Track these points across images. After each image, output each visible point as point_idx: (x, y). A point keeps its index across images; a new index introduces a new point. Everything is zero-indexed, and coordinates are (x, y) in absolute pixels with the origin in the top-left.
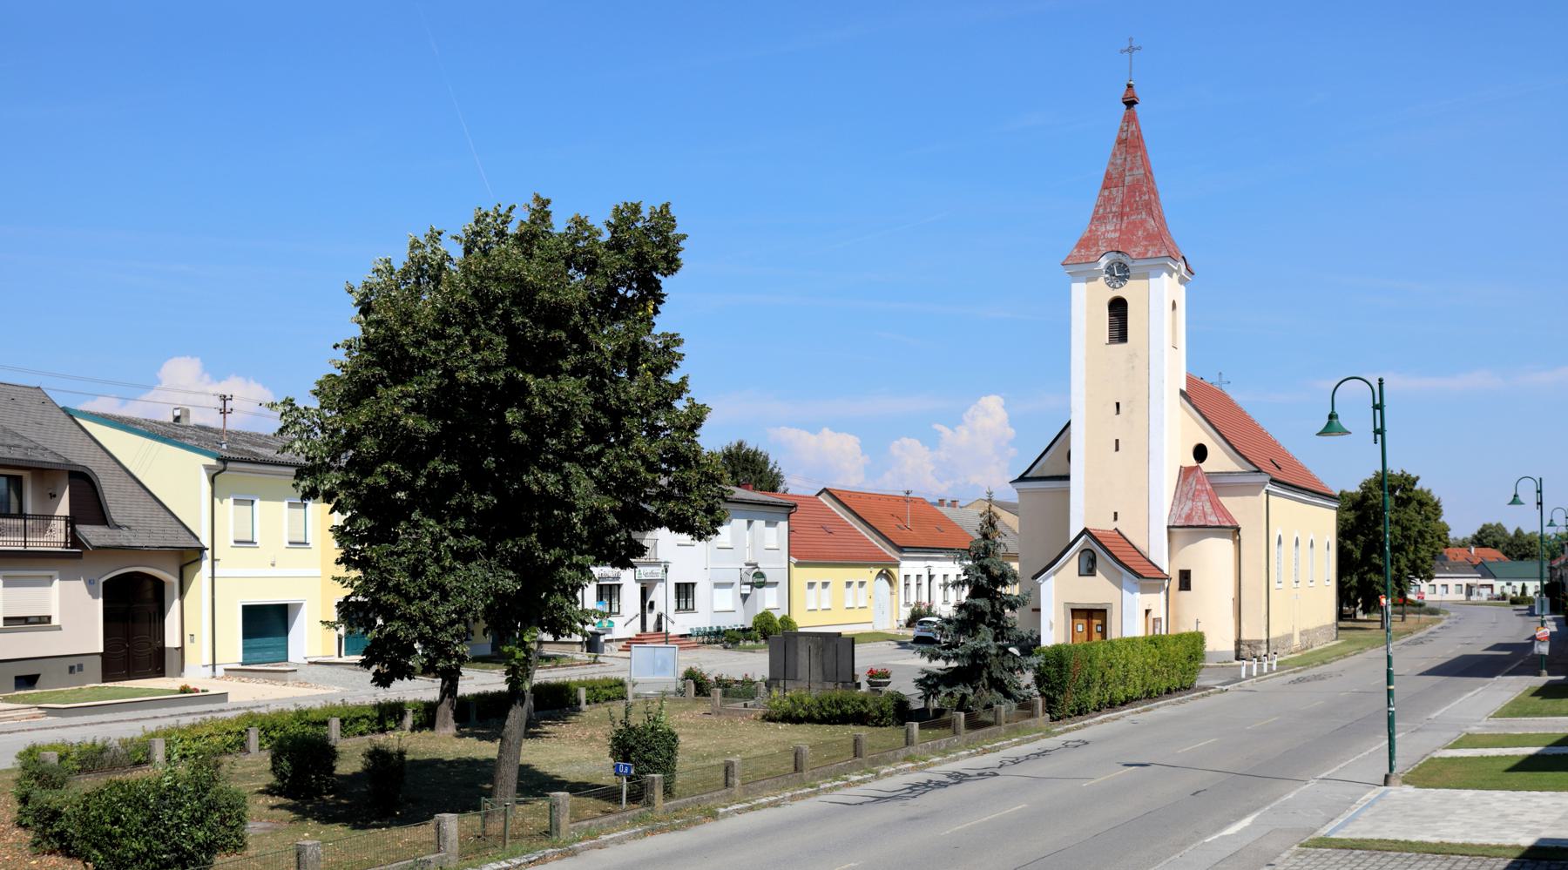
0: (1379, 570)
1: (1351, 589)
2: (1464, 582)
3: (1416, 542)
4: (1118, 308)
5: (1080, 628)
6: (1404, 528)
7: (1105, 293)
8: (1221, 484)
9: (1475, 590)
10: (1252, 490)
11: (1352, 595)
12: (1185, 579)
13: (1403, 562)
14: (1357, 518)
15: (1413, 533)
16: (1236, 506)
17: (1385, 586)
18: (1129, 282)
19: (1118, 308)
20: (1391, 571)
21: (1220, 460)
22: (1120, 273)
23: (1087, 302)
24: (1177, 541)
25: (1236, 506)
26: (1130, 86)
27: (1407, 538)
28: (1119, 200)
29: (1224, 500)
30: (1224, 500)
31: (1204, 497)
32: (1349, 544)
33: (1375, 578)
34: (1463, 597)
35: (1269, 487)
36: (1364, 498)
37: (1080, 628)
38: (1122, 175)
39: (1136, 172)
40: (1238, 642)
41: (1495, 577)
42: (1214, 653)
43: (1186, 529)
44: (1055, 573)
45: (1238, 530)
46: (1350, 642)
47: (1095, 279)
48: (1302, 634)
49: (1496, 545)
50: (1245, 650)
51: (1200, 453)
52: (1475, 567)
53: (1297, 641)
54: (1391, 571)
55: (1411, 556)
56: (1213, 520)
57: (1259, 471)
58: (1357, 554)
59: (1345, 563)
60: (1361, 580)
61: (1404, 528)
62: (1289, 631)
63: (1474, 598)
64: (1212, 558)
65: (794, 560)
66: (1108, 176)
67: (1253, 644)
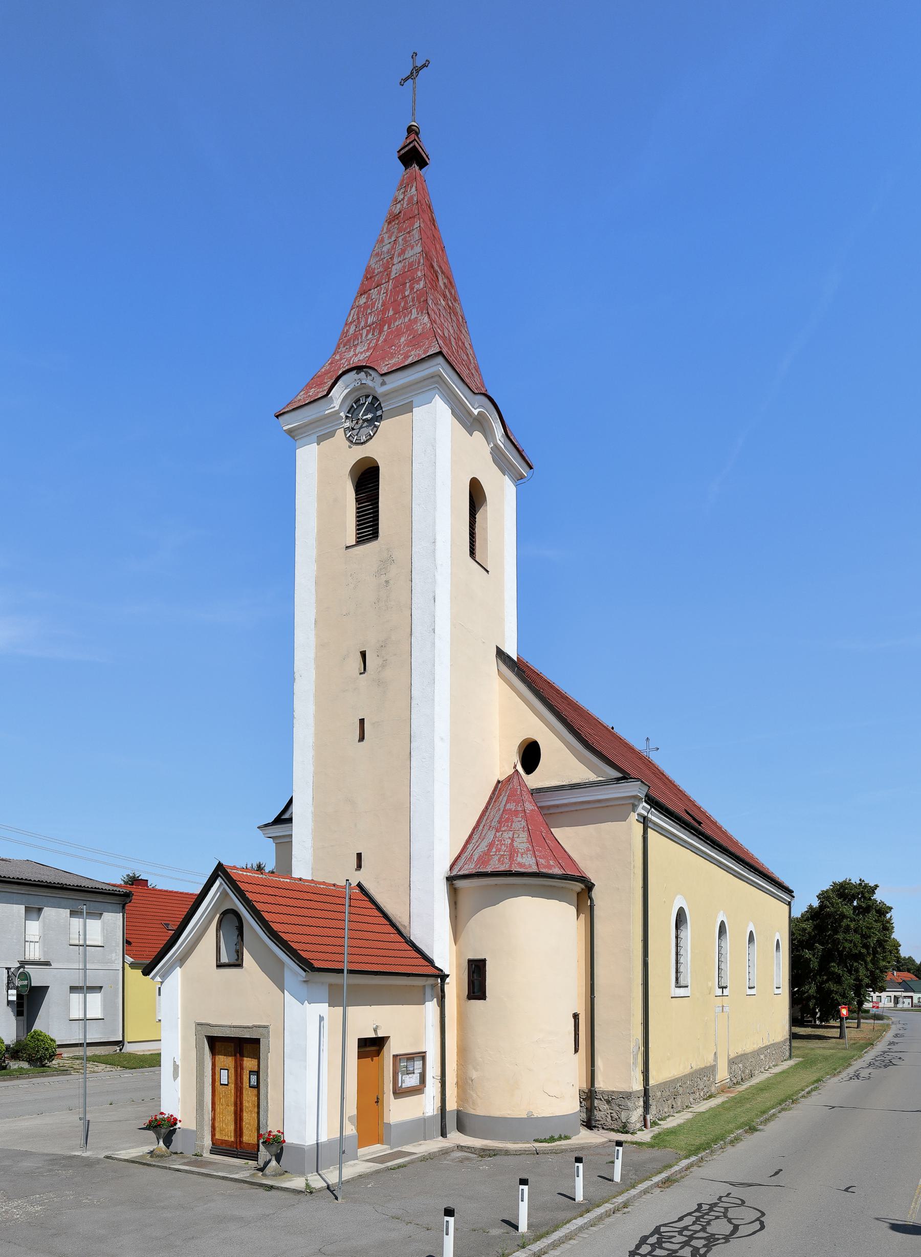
0: (838, 980)
1: (809, 998)
2: (892, 994)
3: (875, 952)
4: (367, 480)
5: (224, 1077)
6: (865, 936)
7: (345, 456)
8: (554, 807)
9: (901, 1000)
10: (612, 811)
11: (811, 1004)
12: (477, 972)
13: (862, 972)
14: (816, 927)
15: (872, 941)
16: (577, 841)
17: (844, 996)
18: (383, 425)
19: (367, 480)
20: (849, 980)
21: (563, 764)
22: (368, 411)
23: (318, 474)
24: (465, 901)
25: (577, 841)
26: (410, 130)
27: (866, 946)
28: (379, 305)
29: (559, 833)
30: (559, 833)
31: (519, 823)
32: (807, 954)
33: (833, 986)
34: (892, 1004)
35: (643, 808)
36: (822, 907)
37: (224, 1077)
38: (387, 268)
39: (409, 253)
40: (589, 1097)
41: (914, 991)
42: (603, 1092)
43: (476, 881)
44: (182, 960)
45: (589, 887)
46: (808, 1063)
47: (331, 434)
48: (732, 1062)
49: (909, 971)
50: (602, 1111)
51: (530, 755)
52: (900, 984)
53: (723, 1074)
54: (849, 980)
55: (870, 966)
56: (527, 862)
57: (625, 777)
58: (815, 964)
59: (799, 973)
60: (819, 989)
61: (865, 936)
62: (709, 1060)
63: (900, 1006)
64: (534, 935)
65: (129, 959)
66: (369, 276)
67: (618, 1100)
